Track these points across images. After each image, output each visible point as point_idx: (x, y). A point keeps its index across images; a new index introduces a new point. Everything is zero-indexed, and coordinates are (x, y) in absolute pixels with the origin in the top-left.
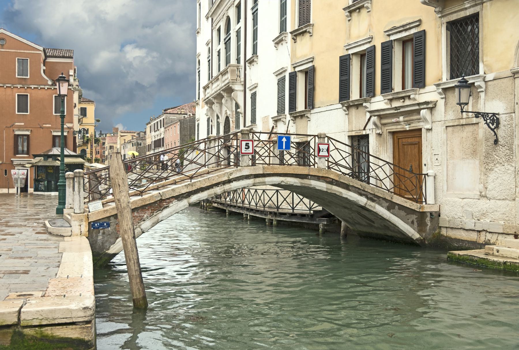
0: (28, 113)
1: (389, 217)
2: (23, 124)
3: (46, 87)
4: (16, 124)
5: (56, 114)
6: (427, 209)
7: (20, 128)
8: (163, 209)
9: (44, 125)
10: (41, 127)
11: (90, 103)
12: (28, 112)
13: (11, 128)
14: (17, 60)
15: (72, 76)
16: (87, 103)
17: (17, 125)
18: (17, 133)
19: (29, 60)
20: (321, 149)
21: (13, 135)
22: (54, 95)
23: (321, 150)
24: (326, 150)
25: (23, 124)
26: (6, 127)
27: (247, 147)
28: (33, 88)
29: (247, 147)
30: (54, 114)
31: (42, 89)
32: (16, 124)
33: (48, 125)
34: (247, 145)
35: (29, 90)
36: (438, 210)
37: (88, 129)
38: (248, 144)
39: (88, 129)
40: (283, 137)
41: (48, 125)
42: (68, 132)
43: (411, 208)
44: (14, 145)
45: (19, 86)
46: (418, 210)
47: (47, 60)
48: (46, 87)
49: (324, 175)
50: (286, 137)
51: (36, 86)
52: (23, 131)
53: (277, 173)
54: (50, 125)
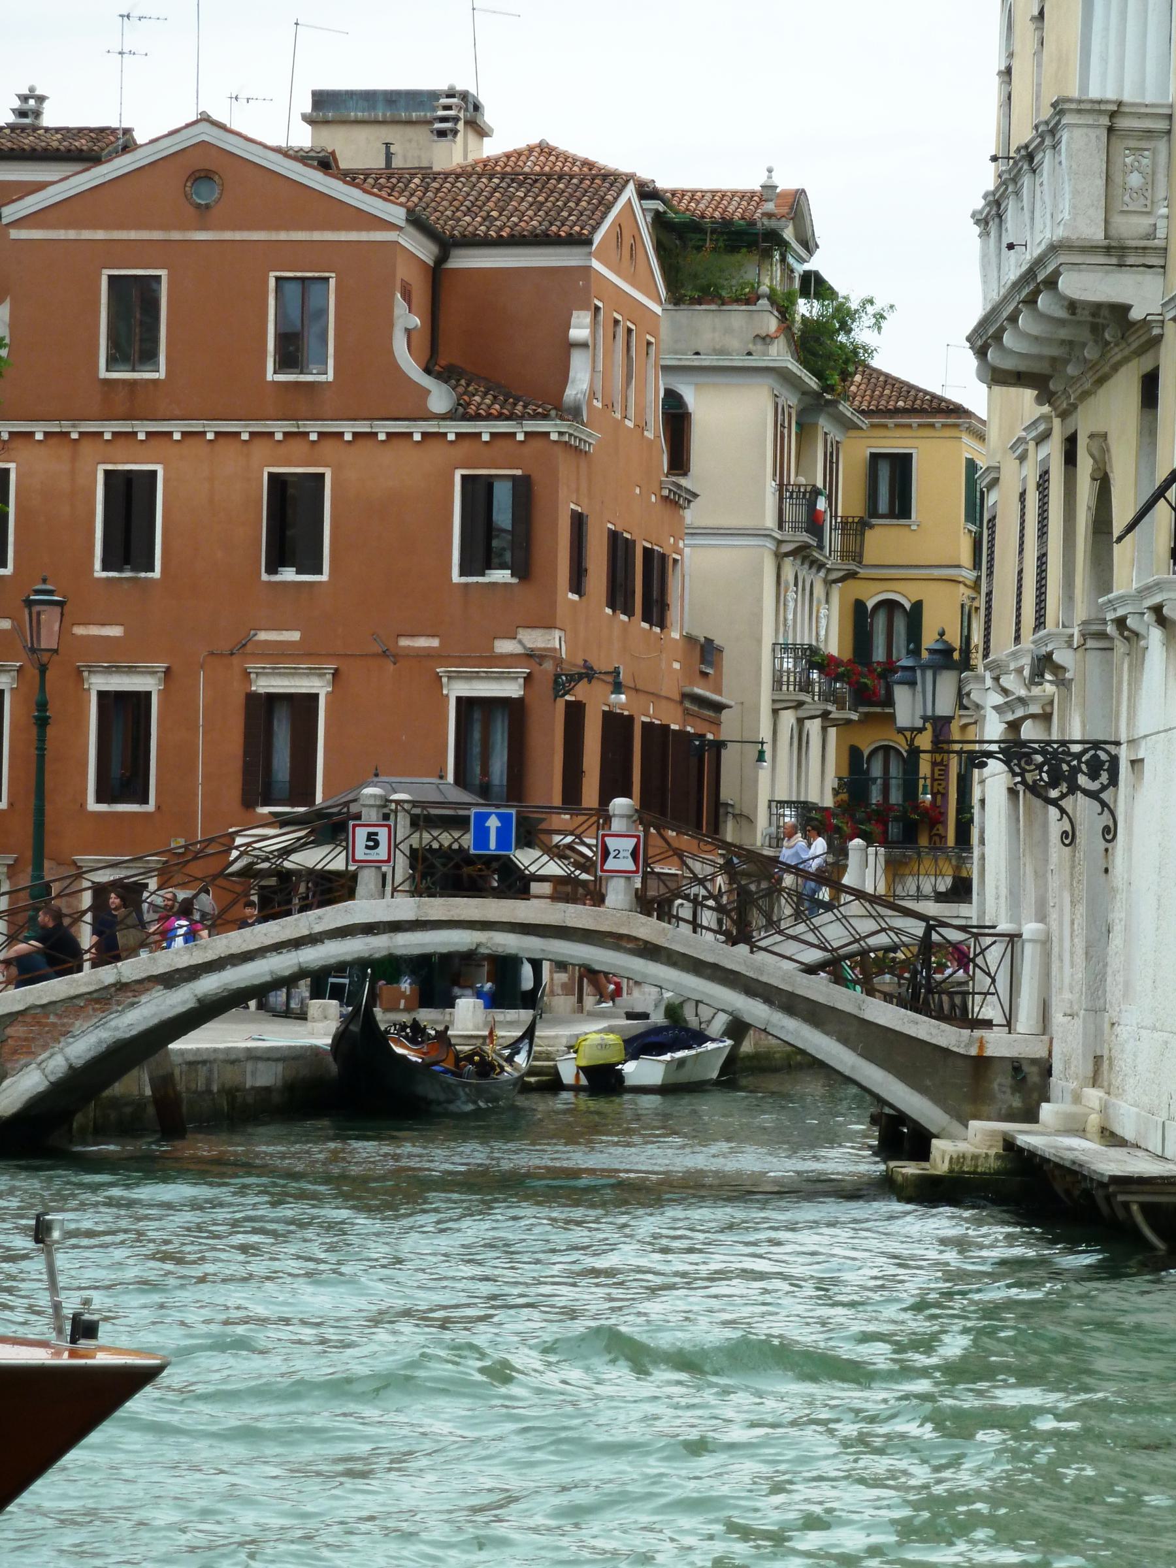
0: (324, 578)
1: (853, 1067)
2: (295, 636)
3: (417, 432)
4: (263, 636)
5: (464, 580)
6: (997, 1044)
7: (279, 655)
8: (123, 1011)
9: (404, 642)
10: (385, 654)
11: (938, 421)
12: (320, 572)
13: (235, 660)
14: (272, 283)
15: (584, 345)
16: (915, 421)
17: (266, 641)
18: (266, 685)
19: (332, 282)
20: (611, 850)
21: (239, 701)
22: (458, 475)
23: (613, 854)
24: (628, 854)
25: (295, 636)
26: (212, 654)
27: (371, 844)
28: (348, 437)
29: (371, 844)
30: (456, 577)
31: (395, 442)
32: (263, 636)
33: (422, 642)
34: (371, 837)
35: (329, 446)
36: (1044, 1054)
37: (918, 606)
38: (376, 834)
39: (918, 606)
40: (488, 815)
41: (422, 642)
42: (528, 679)
43: (934, 1041)
44: (246, 753)
45: (279, 429)
46: (962, 1051)
47: (454, 263)
48: (417, 432)
49: (615, 930)
50: (499, 816)
51: (363, 427)
52: (295, 673)
53: (462, 918)
54: (435, 643)
